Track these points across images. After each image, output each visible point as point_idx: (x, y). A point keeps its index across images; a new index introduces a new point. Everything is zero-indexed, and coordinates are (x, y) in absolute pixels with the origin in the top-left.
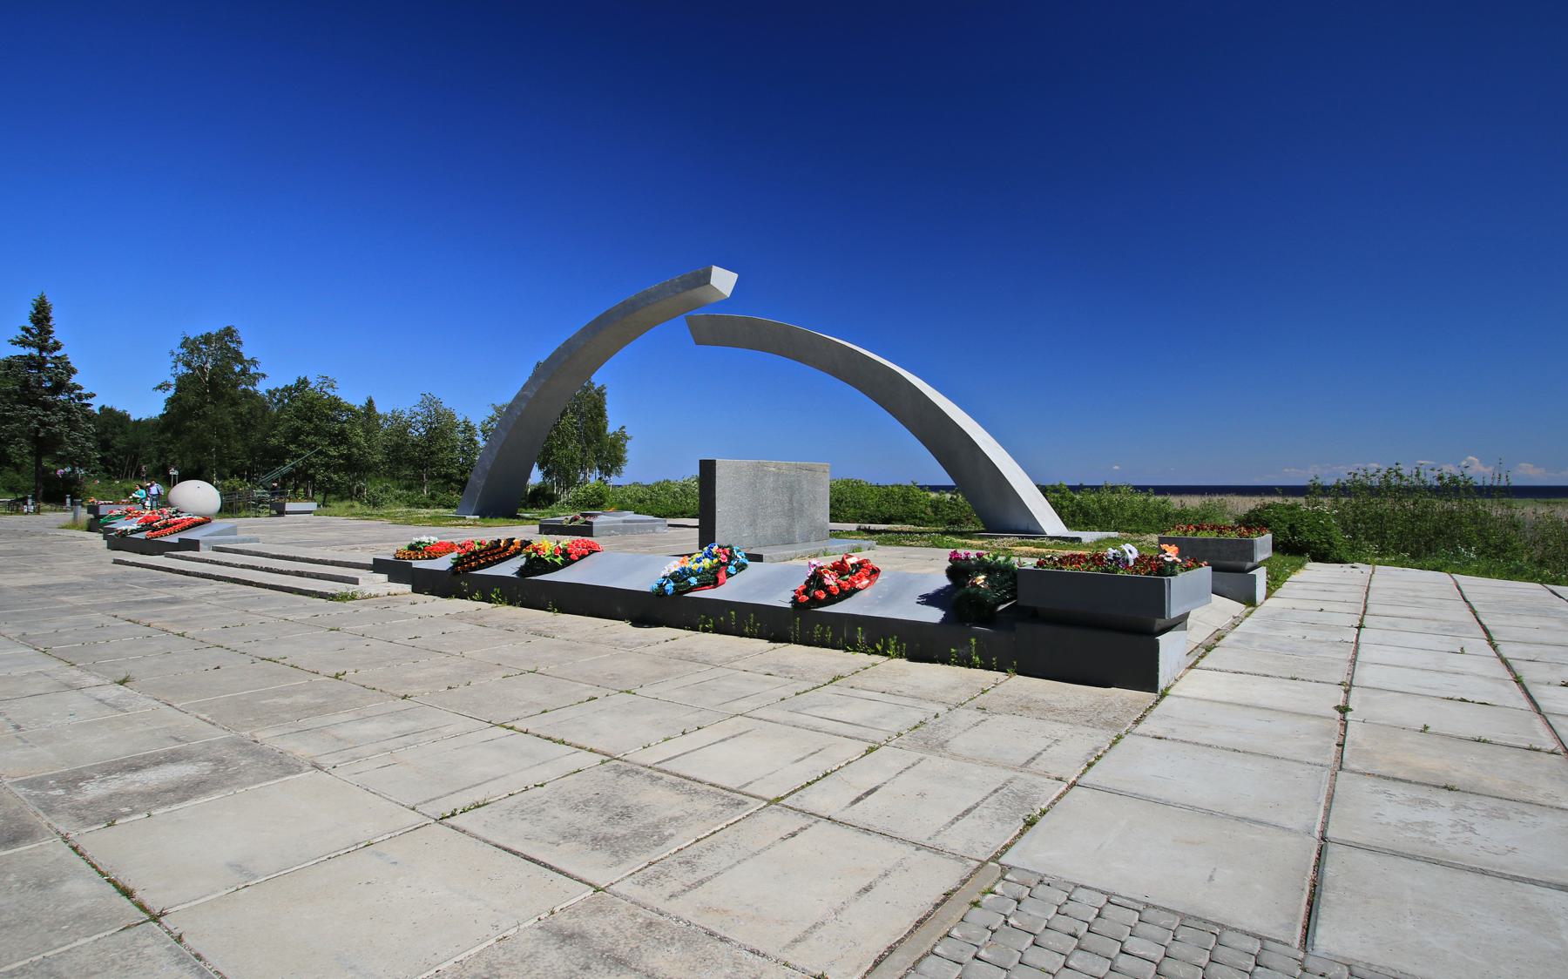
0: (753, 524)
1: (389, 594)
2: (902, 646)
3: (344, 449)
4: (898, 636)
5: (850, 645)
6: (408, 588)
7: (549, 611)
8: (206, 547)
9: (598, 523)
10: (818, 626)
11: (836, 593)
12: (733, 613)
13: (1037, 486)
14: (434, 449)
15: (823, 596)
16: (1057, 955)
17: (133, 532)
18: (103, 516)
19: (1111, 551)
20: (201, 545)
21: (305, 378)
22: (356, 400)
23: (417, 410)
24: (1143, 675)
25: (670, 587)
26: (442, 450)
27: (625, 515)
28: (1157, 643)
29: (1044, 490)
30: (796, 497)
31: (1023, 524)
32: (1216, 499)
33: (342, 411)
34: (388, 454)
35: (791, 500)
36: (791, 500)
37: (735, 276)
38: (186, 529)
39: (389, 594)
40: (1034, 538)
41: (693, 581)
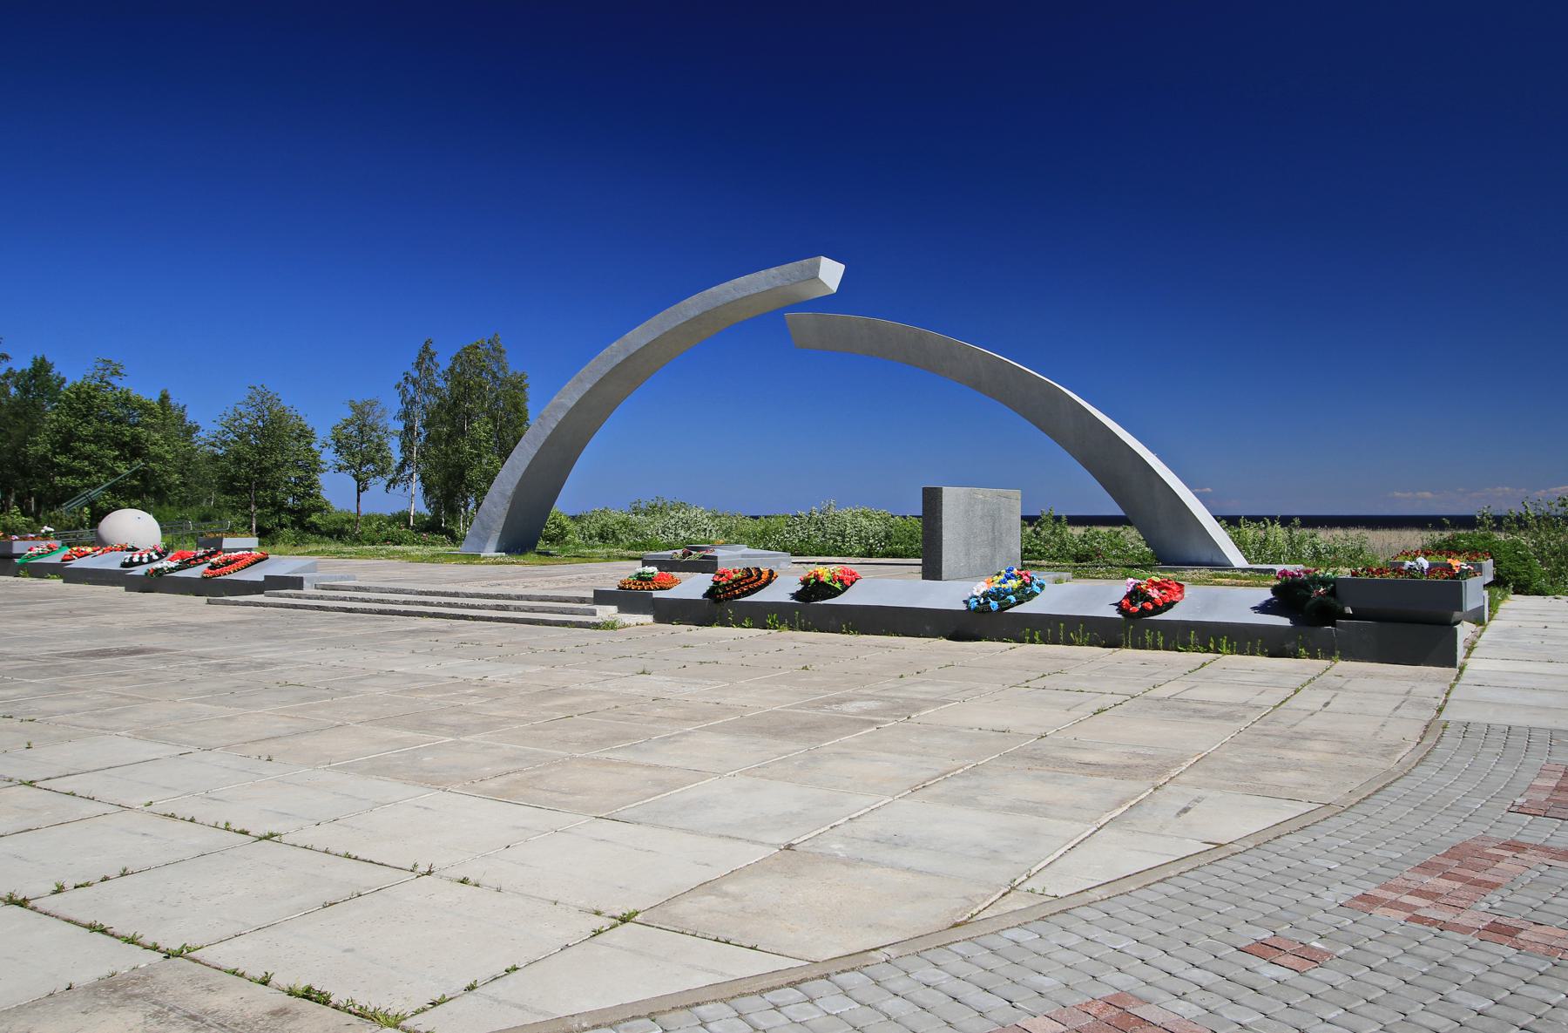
0: (967, 554)
1: (637, 624)
2: (1232, 645)
3: (139, 463)
4: (1228, 636)
5: (1185, 646)
6: (649, 618)
7: (844, 633)
8: (309, 585)
9: (723, 557)
10: (1148, 631)
11: (1161, 605)
12: (1062, 625)
13: (1214, 517)
14: (267, 464)
15: (1151, 607)
16: (1171, 1014)
17: (172, 570)
18: (19, 556)
19: (1408, 563)
20: (305, 582)
21: (43, 359)
22: (151, 396)
23: (242, 409)
24: (1445, 655)
25: (994, 605)
26: (277, 466)
27: (741, 549)
28: (1455, 632)
29: (1218, 518)
30: (997, 525)
31: (1206, 555)
32: (1353, 533)
33: (134, 409)
34: (162, 470)
35: (993, 529)
36: (993, 529)
37: (842, 267)
38: (249, 566)
39: (637, 624)
40: (1226, 570)
41: (1012, 598)
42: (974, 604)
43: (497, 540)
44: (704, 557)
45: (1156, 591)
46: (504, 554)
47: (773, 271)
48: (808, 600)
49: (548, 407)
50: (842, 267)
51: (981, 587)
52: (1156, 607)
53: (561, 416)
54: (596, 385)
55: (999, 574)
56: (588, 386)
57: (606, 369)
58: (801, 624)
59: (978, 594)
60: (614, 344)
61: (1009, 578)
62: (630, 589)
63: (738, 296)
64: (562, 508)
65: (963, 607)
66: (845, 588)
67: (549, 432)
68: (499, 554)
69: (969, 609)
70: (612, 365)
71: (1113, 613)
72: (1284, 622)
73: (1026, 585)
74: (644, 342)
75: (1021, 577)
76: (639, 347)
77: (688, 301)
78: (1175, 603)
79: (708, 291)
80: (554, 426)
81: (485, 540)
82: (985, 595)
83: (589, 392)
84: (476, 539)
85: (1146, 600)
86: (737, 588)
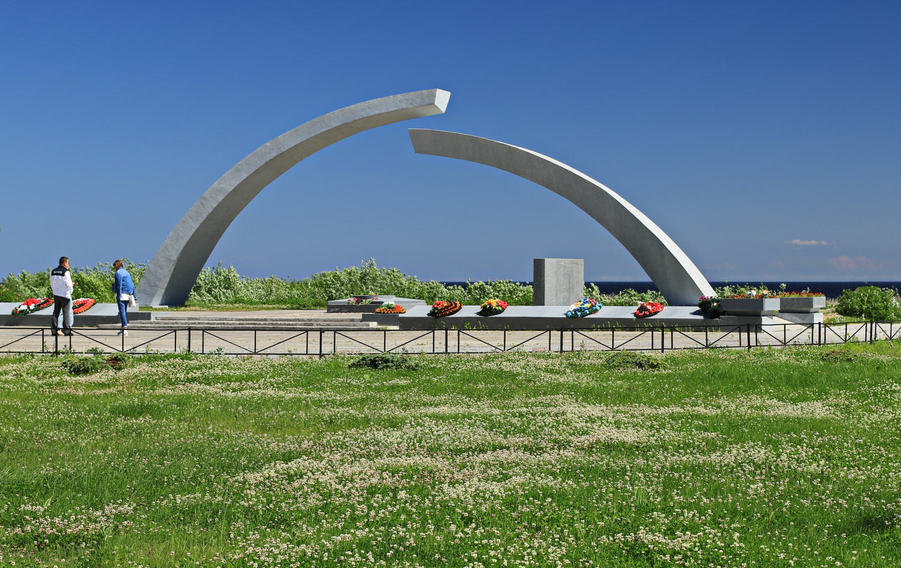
0: (556, 296)
25: (579, 314)
37: (449, 93)
42: (570, 314)
43: (161, 297)
44: (372, 303)
45: (650, 307)
46: (167, 306)
47: (399, 96)
48: (487, 315)
49: (209, 190)
50: (449, 93)
51: (573, 307)
52: (650, 313)
53: (221, 198)
54: (251, 175)
55: (580, 301)
56: (245, 175)
57: (261, 163)
58: (483, 327)
59: (571, 310)
60: (268, 144)
61: (585, 303)
62: (384, 313)
63: (372, 113)
64: (205, 275)
65: (565, 316)
66: (504, 310)
67: (210, 210)
68: (163, 307)
69: (568, 317)
70: (267, 159)
71: (632, 317)
72: (701, 317)
73: (593, 306)
74: (293, 144)
75: (591, 302)
76: (290, 147)
77: (331, 114)
78: (659, 312)
79: (347, 108)
80: (215, 205)
81: (152, 295)
82: (575, 310)
83: (246, 180)
84: (143, 295)
85: (647, 311)
86: (447, 311)
